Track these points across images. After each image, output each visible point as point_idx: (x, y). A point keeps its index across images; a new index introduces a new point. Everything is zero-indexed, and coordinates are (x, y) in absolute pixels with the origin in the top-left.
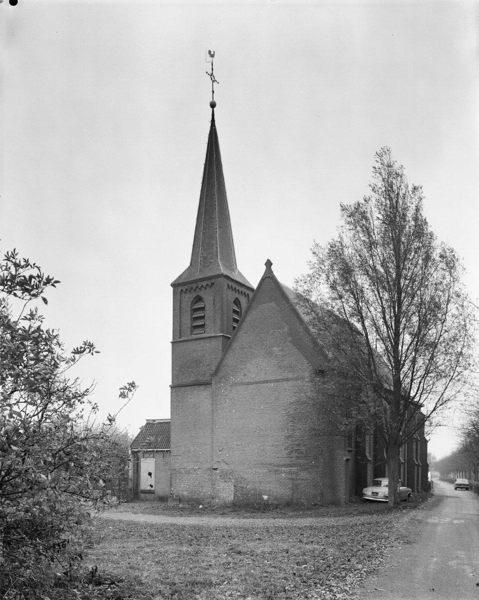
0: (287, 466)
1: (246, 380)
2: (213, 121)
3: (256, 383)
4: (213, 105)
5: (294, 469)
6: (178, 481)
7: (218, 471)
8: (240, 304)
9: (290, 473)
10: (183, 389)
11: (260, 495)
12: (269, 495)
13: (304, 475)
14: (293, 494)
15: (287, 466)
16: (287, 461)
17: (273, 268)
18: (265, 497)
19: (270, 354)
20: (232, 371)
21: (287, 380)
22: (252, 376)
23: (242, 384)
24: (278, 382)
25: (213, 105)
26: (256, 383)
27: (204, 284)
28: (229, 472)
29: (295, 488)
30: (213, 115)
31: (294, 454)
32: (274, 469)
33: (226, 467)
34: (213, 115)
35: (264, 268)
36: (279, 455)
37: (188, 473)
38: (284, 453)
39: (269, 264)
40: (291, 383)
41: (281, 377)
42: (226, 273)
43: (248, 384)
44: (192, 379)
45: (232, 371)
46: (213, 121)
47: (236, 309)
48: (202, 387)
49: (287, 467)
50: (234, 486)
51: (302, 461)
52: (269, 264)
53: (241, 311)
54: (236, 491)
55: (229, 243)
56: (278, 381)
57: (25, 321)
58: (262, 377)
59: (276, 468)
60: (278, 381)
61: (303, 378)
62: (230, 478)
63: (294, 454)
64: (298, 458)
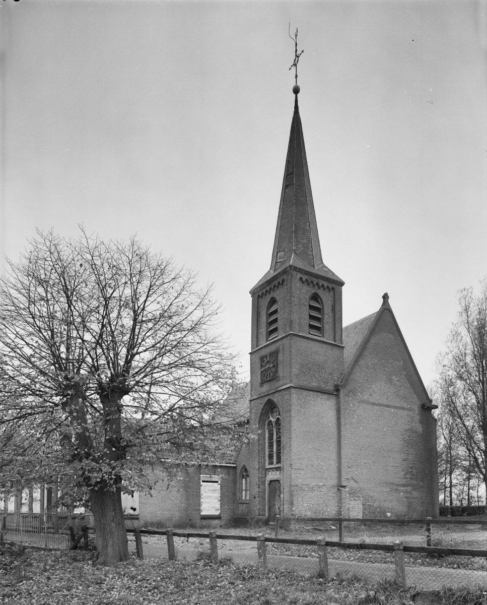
0: (404, 485)
1: (372, 400)
2: (296, 107)
3: (380, 405)
4: (296, 91)
5: (409, 489)
6: (300, 499)
7: (347, 489)
8: (322, 302)
9: (406, 492)
10: (305, 393)
11: (385, 513)
12: (391, 512)
13: (416, 494)
14: (409, 510)
15: (404, 485)
16: (403, 482)
17: (390, 301)
18: (389, 514)
19: (390, 381)
20: (359, 387)
21: (403, 409)
22: (375, 398)
23: (368, 403)
24: (397, 409)
25: (296, 91)
26: (380, 405)
27: (326, 284)
28: (358, 490)
29: (410, 505)
30: (296, 101)
31: (408, 476)
32: (394, 487)
33: (354, 485)
34: (296, 101)
35: (382, 300)
36: (398, 476)
37: (312, 489)
38: (402, 473)
39: (386, 297)
40: (406, 412)
41: (398, 405)
42: (300, 264)
43: (374, 404)
44: (314, 384)
45: (359, 387)
46: (296, 107)
47: (317, 306)
48: (326, 396)
49: (404, 487)
50: (363, 504)
51: (414, 482)
52: (386, 297)
53: (323, 307)
54: (365, 509)
55: (309, 241)
56: (396, 407)
57: (293, 61)
58: (385, 402)
59: (396, 487)
60: (396, 407)
61: (413, 410)
62: (359, 497)
63: (408, 476)
64: (411, 479)
